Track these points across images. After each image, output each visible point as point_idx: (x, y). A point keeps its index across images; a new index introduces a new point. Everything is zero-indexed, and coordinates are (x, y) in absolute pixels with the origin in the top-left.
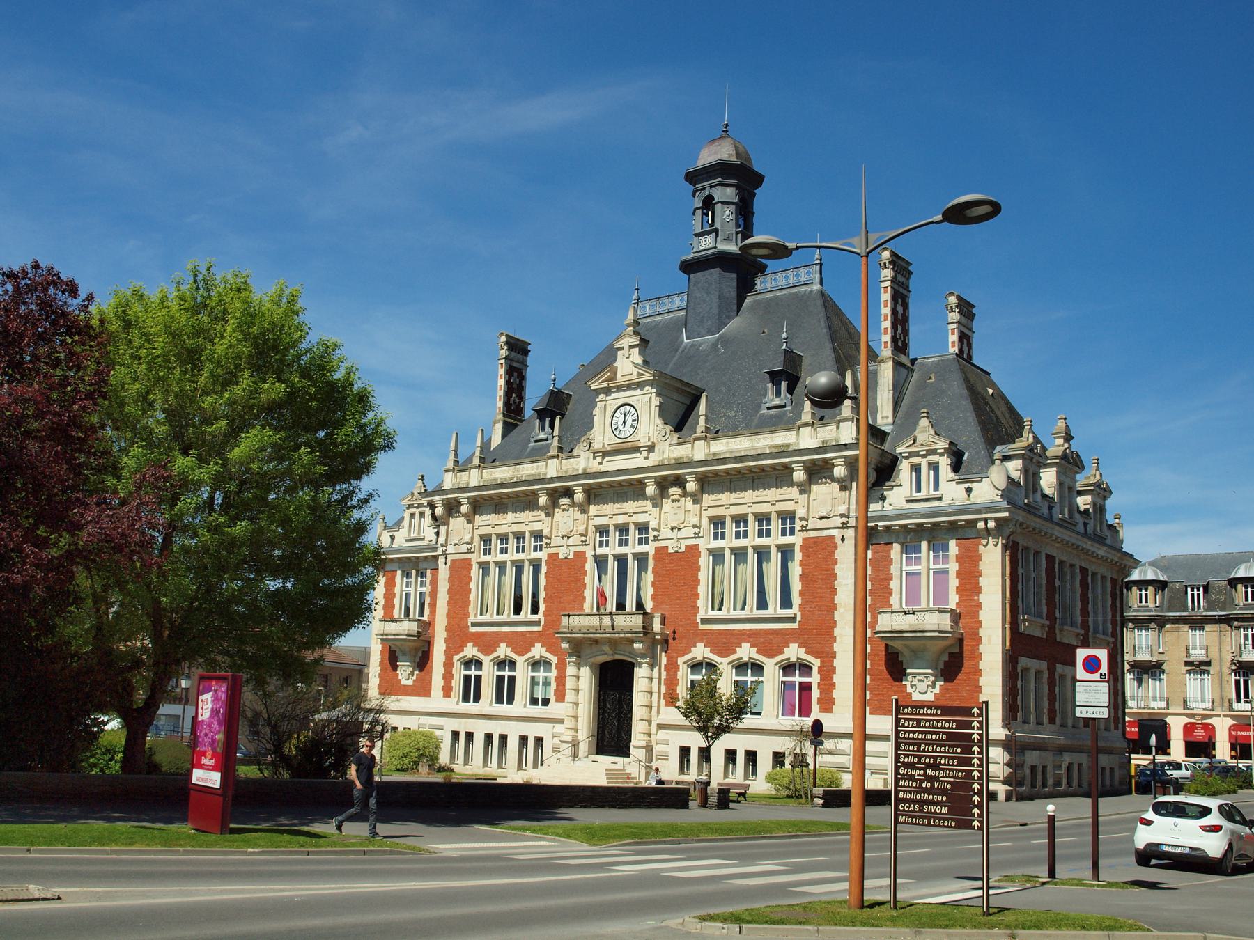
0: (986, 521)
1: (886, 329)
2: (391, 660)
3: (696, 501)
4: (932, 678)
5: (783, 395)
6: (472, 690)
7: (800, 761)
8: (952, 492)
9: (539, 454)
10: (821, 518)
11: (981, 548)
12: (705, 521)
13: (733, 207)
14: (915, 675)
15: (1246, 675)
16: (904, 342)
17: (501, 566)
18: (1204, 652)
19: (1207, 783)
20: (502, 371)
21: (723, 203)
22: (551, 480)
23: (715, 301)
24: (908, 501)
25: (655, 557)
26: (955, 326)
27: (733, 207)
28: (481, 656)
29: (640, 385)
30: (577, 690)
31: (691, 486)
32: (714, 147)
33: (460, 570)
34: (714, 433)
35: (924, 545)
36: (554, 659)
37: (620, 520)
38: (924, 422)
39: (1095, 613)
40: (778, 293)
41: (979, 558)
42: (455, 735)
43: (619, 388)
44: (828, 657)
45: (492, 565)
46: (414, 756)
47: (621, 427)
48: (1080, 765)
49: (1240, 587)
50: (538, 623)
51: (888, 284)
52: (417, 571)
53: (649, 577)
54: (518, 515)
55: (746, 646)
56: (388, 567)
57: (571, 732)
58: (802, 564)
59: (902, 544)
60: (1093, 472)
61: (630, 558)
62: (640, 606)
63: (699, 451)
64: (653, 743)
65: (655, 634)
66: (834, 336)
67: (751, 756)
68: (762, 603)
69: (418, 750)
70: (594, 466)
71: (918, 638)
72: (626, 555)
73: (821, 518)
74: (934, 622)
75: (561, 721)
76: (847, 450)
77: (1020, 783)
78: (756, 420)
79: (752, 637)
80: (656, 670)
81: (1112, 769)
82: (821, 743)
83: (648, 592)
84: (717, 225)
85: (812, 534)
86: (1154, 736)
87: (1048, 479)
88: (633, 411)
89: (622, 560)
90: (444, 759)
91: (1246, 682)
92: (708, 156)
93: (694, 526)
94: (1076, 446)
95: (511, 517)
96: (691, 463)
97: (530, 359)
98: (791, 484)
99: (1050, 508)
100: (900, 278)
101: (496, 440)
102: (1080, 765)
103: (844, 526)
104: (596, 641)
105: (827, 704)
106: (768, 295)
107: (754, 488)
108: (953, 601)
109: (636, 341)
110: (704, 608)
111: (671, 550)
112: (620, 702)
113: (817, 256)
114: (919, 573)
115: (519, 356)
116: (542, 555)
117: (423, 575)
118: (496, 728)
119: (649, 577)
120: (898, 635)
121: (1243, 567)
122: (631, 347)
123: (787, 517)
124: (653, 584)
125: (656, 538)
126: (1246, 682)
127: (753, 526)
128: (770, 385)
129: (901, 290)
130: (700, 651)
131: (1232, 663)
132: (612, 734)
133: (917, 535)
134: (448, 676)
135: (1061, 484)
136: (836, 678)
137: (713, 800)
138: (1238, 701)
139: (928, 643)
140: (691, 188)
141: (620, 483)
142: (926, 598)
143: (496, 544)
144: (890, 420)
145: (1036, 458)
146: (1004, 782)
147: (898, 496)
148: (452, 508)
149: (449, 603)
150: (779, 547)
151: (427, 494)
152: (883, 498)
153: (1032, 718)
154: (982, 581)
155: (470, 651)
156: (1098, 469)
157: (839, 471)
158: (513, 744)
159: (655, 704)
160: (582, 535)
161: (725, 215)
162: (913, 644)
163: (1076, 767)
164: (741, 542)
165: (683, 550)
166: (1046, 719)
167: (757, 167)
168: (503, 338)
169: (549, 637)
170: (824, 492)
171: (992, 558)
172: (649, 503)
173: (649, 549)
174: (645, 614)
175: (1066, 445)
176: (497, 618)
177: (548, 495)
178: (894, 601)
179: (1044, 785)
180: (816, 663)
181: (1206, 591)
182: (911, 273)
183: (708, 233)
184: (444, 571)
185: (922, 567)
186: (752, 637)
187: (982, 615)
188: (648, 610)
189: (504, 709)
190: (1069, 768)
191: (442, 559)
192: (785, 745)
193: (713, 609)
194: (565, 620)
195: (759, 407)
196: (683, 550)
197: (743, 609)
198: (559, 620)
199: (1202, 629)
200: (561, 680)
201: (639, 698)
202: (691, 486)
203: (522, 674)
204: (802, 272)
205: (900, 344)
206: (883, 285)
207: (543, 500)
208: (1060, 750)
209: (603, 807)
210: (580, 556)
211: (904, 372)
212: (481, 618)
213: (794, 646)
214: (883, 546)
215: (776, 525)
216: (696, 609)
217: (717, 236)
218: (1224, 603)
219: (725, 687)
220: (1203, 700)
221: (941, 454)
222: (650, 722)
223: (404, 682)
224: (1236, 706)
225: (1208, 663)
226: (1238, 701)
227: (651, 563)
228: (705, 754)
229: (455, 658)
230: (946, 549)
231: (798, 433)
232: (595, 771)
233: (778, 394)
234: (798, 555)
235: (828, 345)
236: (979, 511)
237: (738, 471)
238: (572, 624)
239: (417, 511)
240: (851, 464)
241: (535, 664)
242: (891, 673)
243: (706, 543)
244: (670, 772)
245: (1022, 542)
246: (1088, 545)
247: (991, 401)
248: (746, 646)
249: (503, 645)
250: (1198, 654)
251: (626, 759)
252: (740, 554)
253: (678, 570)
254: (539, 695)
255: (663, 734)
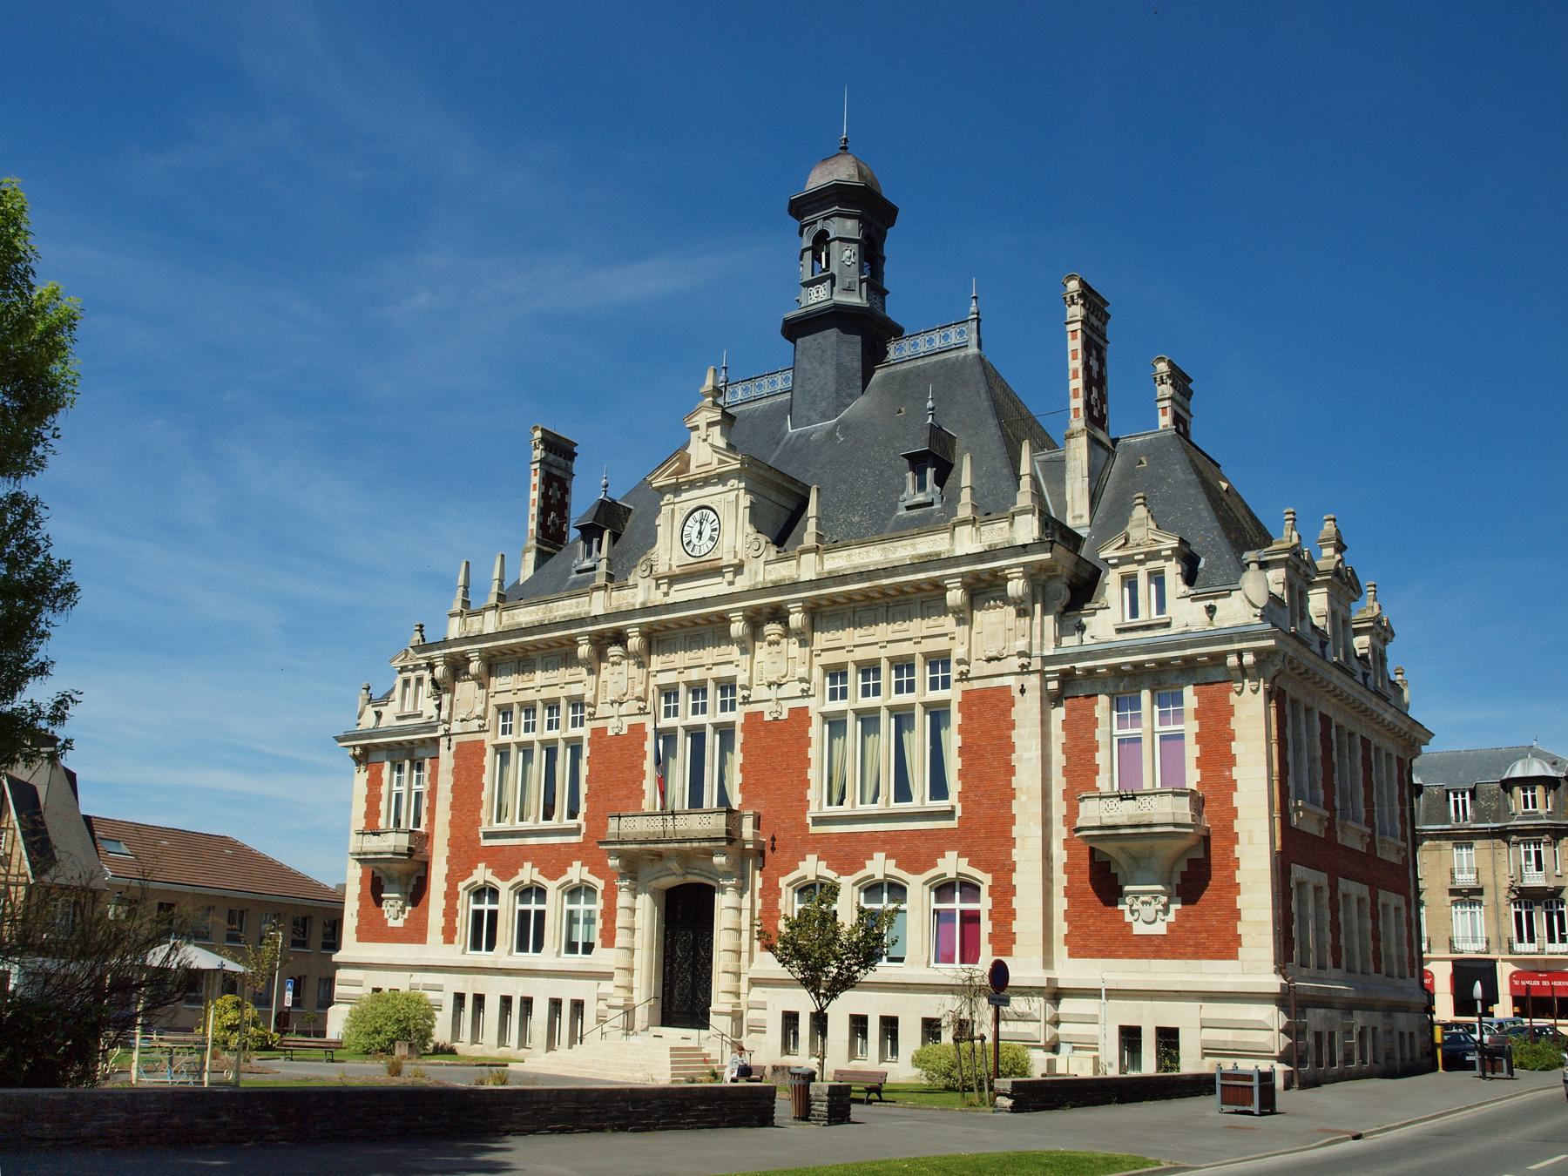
0: (1240, 654)
1: (1076, 390)
2: (375, 889)
3: (804, 643)
4: (1164, 899)
5: (928, 489)
6: (484, 932)
7: (963, 1029)
8: (1186, 614)
9: (582, 588)
10: (989, 660)
11: (1233, 696)
12: (817, 673)
13: (855, 247)
14: (1137, 895)
15: (1529, 906)
16: (1101, 411)
17: (526, 749)
18: (1473, 876)
19: (1535, 1052)
20: (536, 480)
21: (841, 240)
22: (595, 619)
23: (832, 371)
24: (1119, 631)
25: (744, 728)
26: (1167, 403)
27: (855, 247)
28: (497, 882)
29: (722, 478)
30: (632, 930)
31: (796, 620)
32: (828, 167)
33: (469, 757)
34: (825, 545)
35: (1145, 695)
36: (600, 884)
37: (695, 675)
38: (1140, 512)
39: (1380, 805)
40: (920, 362)
41: (1230, 711)
42: (459, 998)
43: (692, 485)
44: (1003, 870)
45: (513, 749)
46: (391, 1028)
47: (695, 541)
48: (1374, 1029)
49: (1517, 791)
50: (577, 831)
51: (1078, 326)
52: (412, 762)
53: (737, 758)
54: (550, 674)
55: (879, 856)
56: (373, 757)
57: (623, 993)
58: (961, 730)
59: (1111, 696)
60: (1370, 603)
61: (709, 731)
62: (723, 798)
63: (808, 568)
64: (744, 1008)
65: (744, 842)
66: (998, 410)
67: (890, 1026)
68: (903, 793)
69: (398, 1021)
70: (657, 598)
71: (1143, 833)
72: (703, 727)
73: (989, 660)
74: (1167, 810)
75: (608, 976)
76: (1026, 553)
77: (1302, 1061)
78: (891, 523)
79: (889, 843)
80: (747, 896)
81: (1411, 1034)
82: (1007, 1002)
83: (735, 779)
84: (834, 269)
85: (976, 685)
86: (1478, 984)
87: (1318, 602)
88: (712, 516)
89: (697, 735)
90: (441, 1032)
91: (1529, 916)
92: (818, 179)
93: (801, 680)
94: (1352, 560)
95: (539, 677)
96: (795, 586)
97: (577, 466)
98: (944, 610)
99: (1323, 645)
100: (1093, 320)
101: (527, 571)
102: (1374, 1029)
103: (1024, 670)
104: (659, 855)
105: (1004, 940)
106: (905, 366)
107: (924, 616)
108: (1193, 778)
109: (716, 415)
110: (817, 802)
111: (767, 718)
112: (695, 948)
113: (973, 309)
114: (1139, 740)
115: (561, 460)
116: (584, 732)
117: (420, 767)
118: (517, 988)
119: (737, 758)
120: (1110, 832)
121: (1519, 764)
122: (710, 425)
123: (939, 661)
124: (743, 769)
125: (746, 701)
126: (1529, 916)
127: (888, 677)
128: (910, 475)
129: (1095, 337)
130: (812, 867)
131: (1511, 890)
132: (683, 996)
133: (1129, 682)
134: (450, 913)
135: (1333, 614)
136: (1016, 903)
137: (820, 1107)
138: (1521, 940)
139: (1157, 843)
140: (797, 224)
141: (692, 619)
142: (1150, 776)
143: (519, 718)
144: (1086, 520)
145: (1303, 568)
146: (1280, 1059)
147: (1104, 623)
148: (457, 667)
149: (453, 806)
150: (927, 706)
151: (423, 647)
152: (1081, 628)
153: (1312, 960)
154: (1236, 747)
155: (482, 874)
156: (1375, 599)
157: (1016, 587)
158: (541, 1011)
159: (745, 947)
160: (639, 699)
161: (844, 257)
162: (1135, 846)
163: (1369, 1030)
164: (871, 702)
165: (785, 716)
166: (1329, 961)
167: (888, 194)
168: (538, 434)
169: (590, 853)
170: (994, 622)
171: (1250, 712)
172: (735, 649)
173: (737, 716)
174: (730, 811)
175: (1338, 557)
176: (519, 826)
177: (591, 642)
178: (1102, 782)
179: (1332, 1063)
180: (985, 880)
181: (1473, 797)
182: (1108, 316)
183: (820, 281)
184: (446, 759)
185: (1143, 730)
186: (889, 843)
187: (1238, 800)
188: (735, 807)
189: (529, 959)
190: (1361, 1035)
191: (444, 742)
192: (943, 1007)
193: (830, 803)
194: (613, 824)
195: (895, 507)
196: (785, 716)
197: (875, 801)
198: (606, 825)
199: (1470, 846)
200: (609, 914)
201: (722, 940)
202: (796, 620)
203: (555, 907)
204: (952, 332)
205: (1096, 413)
206: (1070, 328)
207: (583, 650)
208: (1349, 1007)
209: (601, 1129)
210: (637, 730)
211: (1103, 453)
212: (497, 827)
213: (951, 855)
214: (1082, 701)
215: (922, 674)
216: (805, 804)
217: (833, 284)
218: (1497, 811)
219: (847, 908)
220: (1474, 940)
221: (1167, 558)
222: (738, 975)
223: (391, 923)
224: (1518, 947)
225: (1480, 891)
226: (1521, 940)
227: (739, 737)
228: (820, 1022)
229: (461, 885)
230: (1178, 699)
231: (952, 536)
232: (646, 1058)
233: (921, 486)
234: (956, 717)
235: (992, 422)
236: (1229, 639)
237: (864, 594)
238: (624, 830)
239: (412, 676)
240: (1033, 575)
241: (574, 892)
242: (1098, 892)
243: (820, 704)
244: (765, 1051)
245: (1291, 691)
246: (1373, 703)
247: (1225, 496)
248: (879, 856)
249: (528, 865)
250: (1466, 879)
251: (703, 1032)
252: (869, 720)
253: (776, 745)
254: (580, 938)
255: (758, 994)
